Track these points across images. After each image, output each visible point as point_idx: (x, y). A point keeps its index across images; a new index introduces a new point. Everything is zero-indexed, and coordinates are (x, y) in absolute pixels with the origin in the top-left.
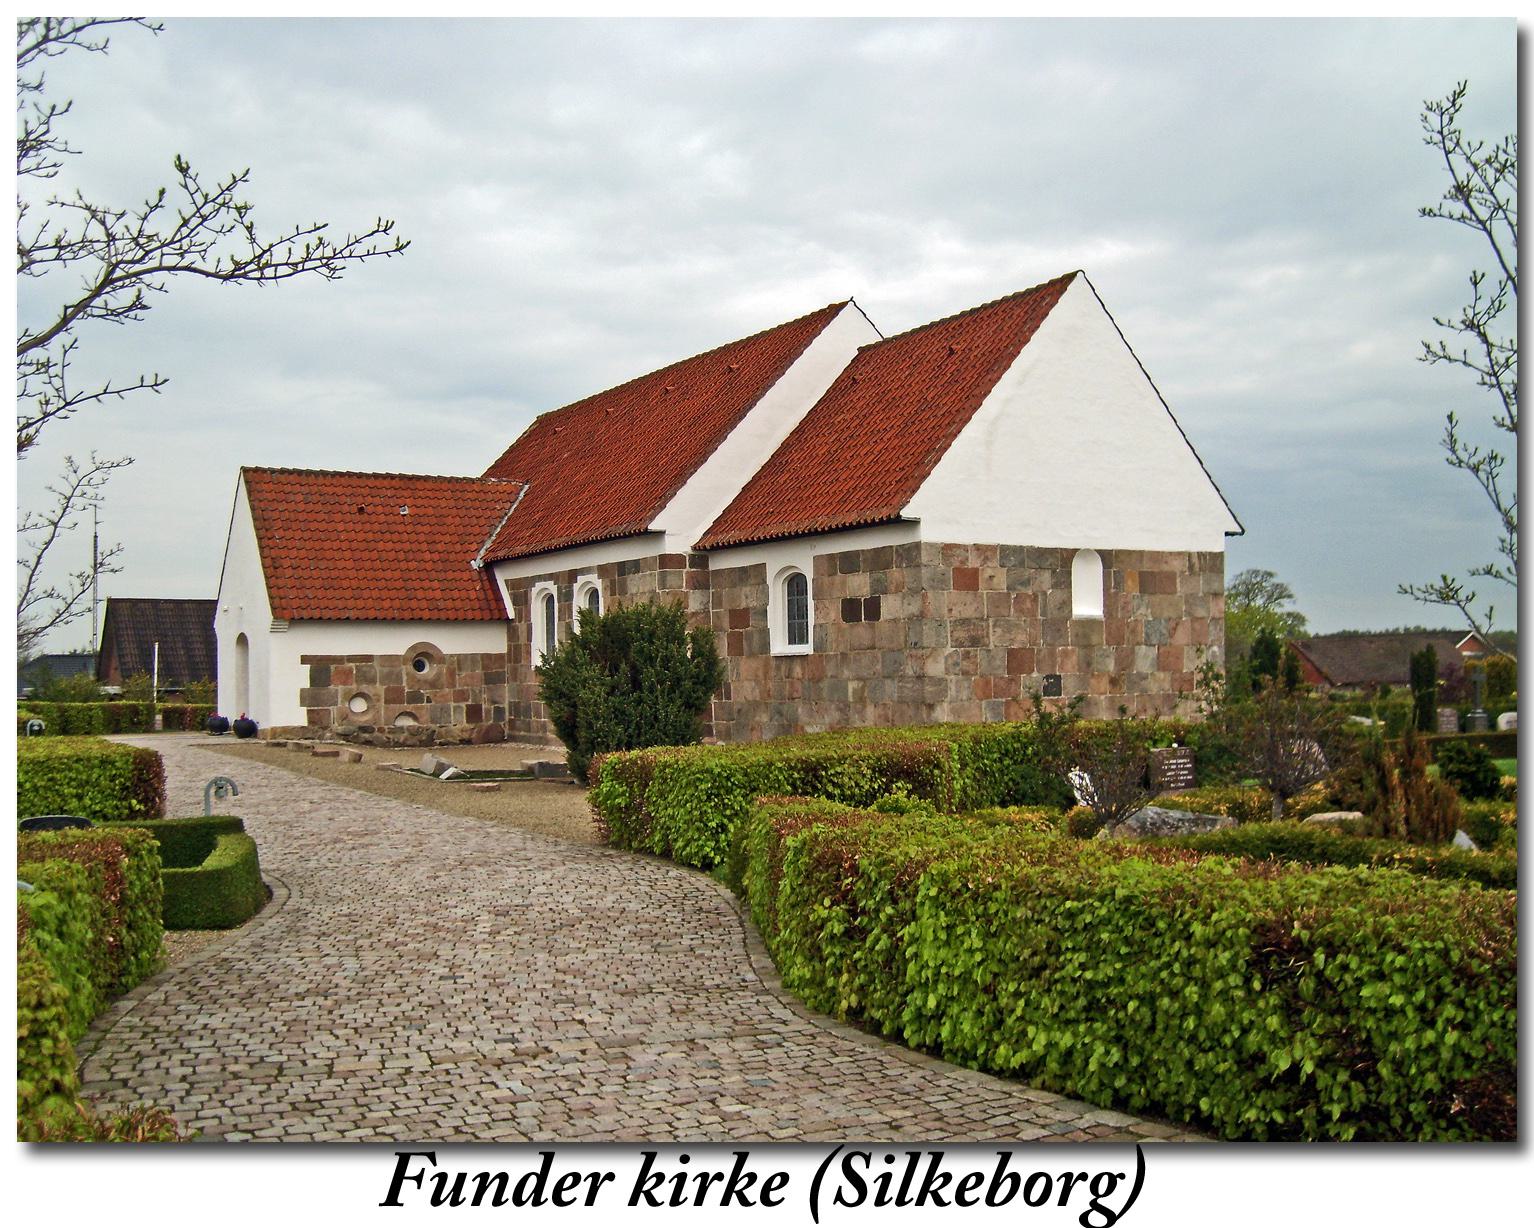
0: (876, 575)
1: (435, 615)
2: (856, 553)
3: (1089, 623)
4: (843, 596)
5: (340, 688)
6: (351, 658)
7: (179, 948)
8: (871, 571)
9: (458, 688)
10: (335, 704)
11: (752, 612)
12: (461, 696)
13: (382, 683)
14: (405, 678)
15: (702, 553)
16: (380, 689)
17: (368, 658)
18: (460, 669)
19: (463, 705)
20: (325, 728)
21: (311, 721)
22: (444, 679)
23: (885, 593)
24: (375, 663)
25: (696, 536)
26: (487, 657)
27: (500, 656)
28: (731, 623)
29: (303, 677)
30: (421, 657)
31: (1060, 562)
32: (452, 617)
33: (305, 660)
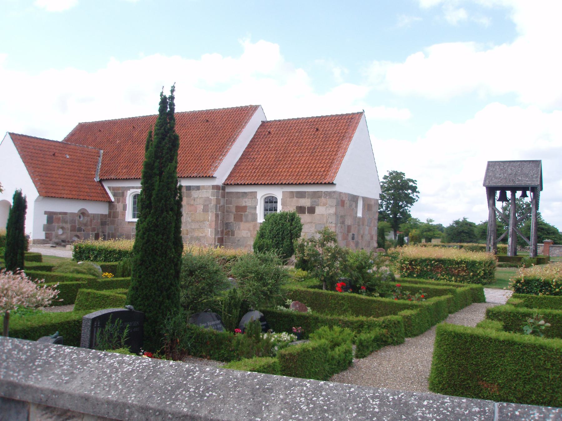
0: (313, 200)
1: (90, 198)
2: (305, 192)
3: (359, 218)
4: (297, 205)
5: (56, 224)
6: (61, 213)
7: (450, 315)
8: (311, 198)
9: (93, 226)
10: (54, 231)
11: (248, 208)
12: (93, 230)
13: (70, 224)
14: (77, 222)
15: (226, 185)
16: (68, 226)
17: (65, 214)
18: (94, 219)
19: (94, 233)
20: (50, 240)
21: (46, 237)
22: (89, 223)
23: (318, 205)
24: (68, 216)
25: (223, 181)
26: (102, 215)
27: (106, 215)
28: (236, 210)
29: (44, 220)
30: (83, 213)
31: (354, 199)
32: (101, 200)
33: (46, 213)
